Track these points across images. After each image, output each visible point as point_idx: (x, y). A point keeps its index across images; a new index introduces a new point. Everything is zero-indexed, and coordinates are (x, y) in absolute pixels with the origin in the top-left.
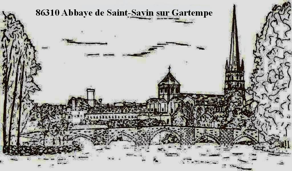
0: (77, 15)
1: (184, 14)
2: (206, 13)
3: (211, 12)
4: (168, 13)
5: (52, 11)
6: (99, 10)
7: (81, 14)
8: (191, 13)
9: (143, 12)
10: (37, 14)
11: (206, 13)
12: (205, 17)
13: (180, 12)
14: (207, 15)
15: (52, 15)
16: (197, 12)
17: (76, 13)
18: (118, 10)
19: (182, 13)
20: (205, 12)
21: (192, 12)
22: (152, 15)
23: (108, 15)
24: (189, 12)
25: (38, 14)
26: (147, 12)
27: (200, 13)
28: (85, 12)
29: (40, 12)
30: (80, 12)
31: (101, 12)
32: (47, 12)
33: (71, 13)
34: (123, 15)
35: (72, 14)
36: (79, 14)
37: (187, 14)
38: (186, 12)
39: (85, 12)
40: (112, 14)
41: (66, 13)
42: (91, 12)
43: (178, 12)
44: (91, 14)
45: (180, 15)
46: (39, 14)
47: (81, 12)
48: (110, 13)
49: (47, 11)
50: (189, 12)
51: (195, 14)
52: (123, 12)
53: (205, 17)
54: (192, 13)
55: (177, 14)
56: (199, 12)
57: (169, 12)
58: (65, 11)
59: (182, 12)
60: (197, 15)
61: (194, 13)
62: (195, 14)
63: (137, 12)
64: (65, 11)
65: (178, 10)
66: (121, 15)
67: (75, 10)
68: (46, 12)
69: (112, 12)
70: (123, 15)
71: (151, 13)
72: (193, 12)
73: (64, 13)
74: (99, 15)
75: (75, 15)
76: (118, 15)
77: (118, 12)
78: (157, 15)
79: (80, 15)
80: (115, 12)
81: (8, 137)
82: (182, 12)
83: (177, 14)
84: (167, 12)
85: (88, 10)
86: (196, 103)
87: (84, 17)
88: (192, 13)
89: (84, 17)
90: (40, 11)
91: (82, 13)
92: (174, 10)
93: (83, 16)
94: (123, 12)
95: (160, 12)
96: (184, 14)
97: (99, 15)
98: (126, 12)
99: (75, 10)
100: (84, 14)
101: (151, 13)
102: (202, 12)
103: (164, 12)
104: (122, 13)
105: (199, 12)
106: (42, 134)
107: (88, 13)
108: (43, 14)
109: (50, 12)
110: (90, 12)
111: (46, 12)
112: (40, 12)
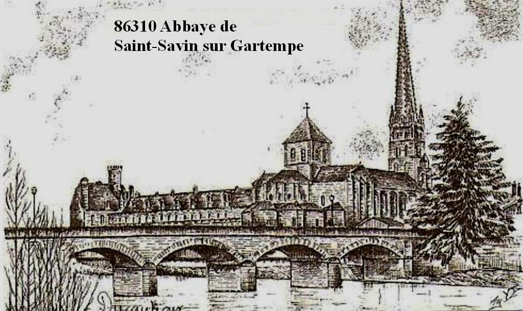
0: (189, 30)
1: (252, 48)
2: (292, 46)
3: (300, 45)
4: (224, 46)
5: (144, 23)
6: (227, 22)
7: (195, 29)
8: (264, 46)
9: (178, 45)
10: (115, 29)
11: (292, 46)
12: (290, 53)
13: (245, 45)
14: (294, 49)
15: (144, 30)
16: (275, 45)
17: (187, 27)
18: (134, 41)
19: (249, 45)
20: (290, 45)
21: (267, 45)
22: (196, 49)
23: (116, 49)
24: (262, 44)
25: (118, 29)
26: (186, 45)
27: (282, 46)
28: (202, 25)
29: (122, 26)
30: (193, 26)
31: (232, 26)
32: (135, 25)
33: (177, 27)
34: (144, 50)
35: (179, 29)
36: (192, 28)
37: (258, 48)
38: (257, 46)
39: (202, 25)
40: (124, 47)
41: (168, 28)
42: (212, 26)
43: (242, 45)
44: (213, 29)
45: (246, 50)
46: (121, 29)
47: (195, 26)
48: (121, 46)
49: (134, 23)
50: (262, 44)
51: (273, 48)
52: (144, 45)
53: (290, 53)
54: (267, 47)
55: (240, 48)
56: (280, 45)
57: (225, 45)
58: (166, 23)
59: (249, 45)
60: (275, 50)
61: (271, 46)
62: (273, 48)
63: (169, 45)
64: (166, 23)
65: (241, 41)
66: (139, 50)
67: (185, 22)
68: (132, 25)
69: (123, 45)
70: (144, 50)
71: (194, 46)
72: (269, 45)
73: (165, 27)
74: (227, 30)
75: (185, 30)
76: (134, 50)
77: (134, 45)
78: (204, 50)
79: (193, 30)
80: (129, 45)
81: (433, 227)
82: (249, 45)
83: (240, 48)
84: (221, 45)
85: (207, 22)
86: (187, 200)
87: (201, 34)
88: (267, 47)
89: (201, 34)
90: (121, 23)
91: (197, 26)
92: (235, 41)
93: (199, 32)
94: (144, 45)
95: (210, 45)
96: (252, 48)
97: (227, 30)
98: (149, 44)
99: (185, 22)
100: (200, 28)
101: (194, 46)
102: (284, 45)
103: (216, 45)
104: (141, 46)
105: (279, 44)
106: (153, 222)
107: (208, 26)
108: (127, 28)
109: (140, 25)
110: (211, 26)
111: (132, 25)
112: (122, 26)
